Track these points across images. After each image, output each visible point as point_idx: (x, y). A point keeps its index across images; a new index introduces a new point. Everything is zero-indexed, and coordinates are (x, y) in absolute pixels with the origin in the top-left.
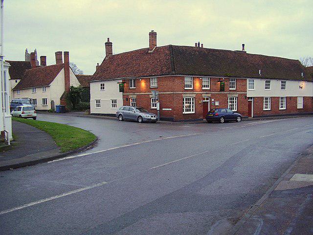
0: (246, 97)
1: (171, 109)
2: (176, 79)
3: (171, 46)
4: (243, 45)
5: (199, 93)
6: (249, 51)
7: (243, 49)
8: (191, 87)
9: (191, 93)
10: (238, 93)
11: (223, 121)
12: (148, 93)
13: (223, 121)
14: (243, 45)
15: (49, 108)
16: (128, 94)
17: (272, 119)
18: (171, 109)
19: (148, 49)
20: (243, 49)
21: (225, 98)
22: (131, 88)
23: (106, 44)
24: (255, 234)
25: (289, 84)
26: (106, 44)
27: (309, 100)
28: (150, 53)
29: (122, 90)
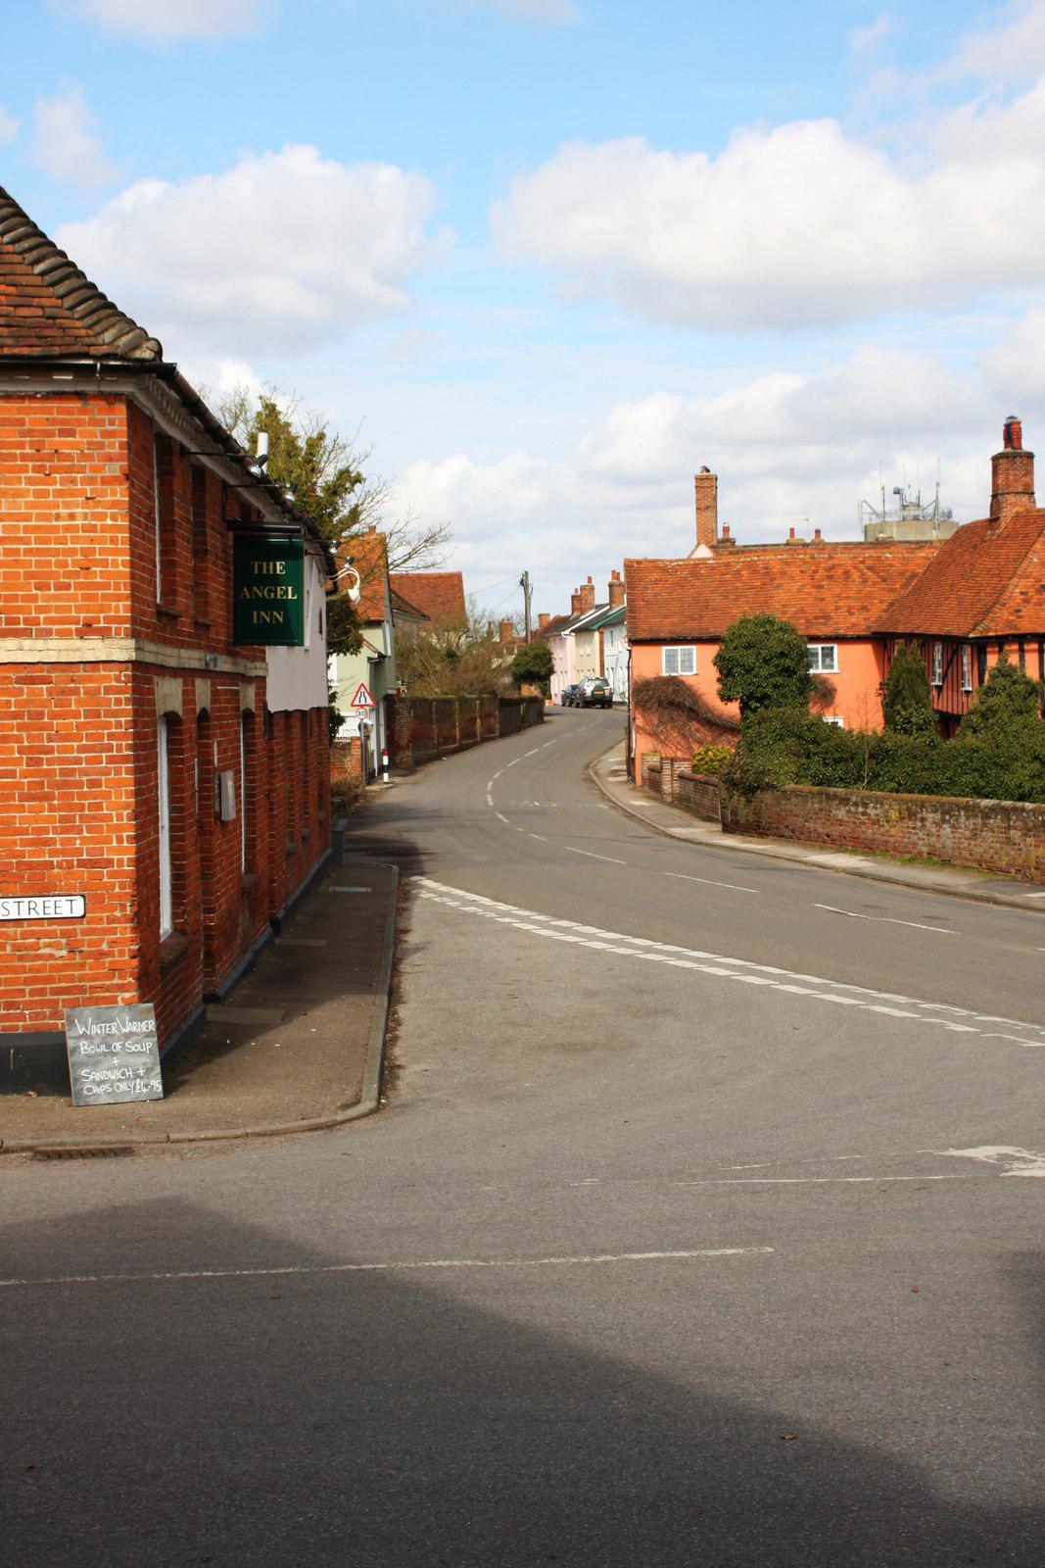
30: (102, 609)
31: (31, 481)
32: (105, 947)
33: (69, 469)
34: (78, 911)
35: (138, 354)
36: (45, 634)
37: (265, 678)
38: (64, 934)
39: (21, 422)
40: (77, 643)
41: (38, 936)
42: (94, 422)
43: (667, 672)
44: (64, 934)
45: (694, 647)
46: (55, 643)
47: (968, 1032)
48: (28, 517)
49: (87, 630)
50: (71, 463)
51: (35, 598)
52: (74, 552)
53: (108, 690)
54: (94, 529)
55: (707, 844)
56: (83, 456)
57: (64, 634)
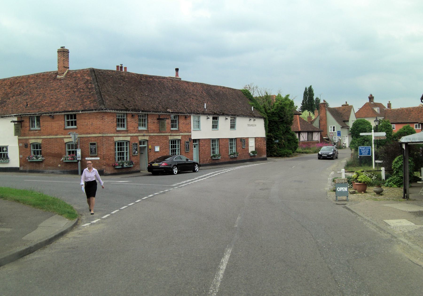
0: (190, 139)
1: (99, 158)
2: (106, 117)
3: (93, 71)
4: (177, 70)
5: (135, 135)
6: (184, 76)
7: (177, 75)
8: (176, 128)
9: (124, 135)
10: (181, 134)
11: (175, 171)
12: (62, 136)
13: (175, 171)
14: (177, 70)
15: (270, 155)
16: (28, 137)
17: (236, 166)
18: (99, 158)
19: (57, 74)
20: (177, 75)
21: (166, 141)
22: (32, 129)
23: (388, 104)
24: (421, 263)
25: (240, 122)
26: (388, 104)
27: (261, 141)
28: (60, 80)
29: (17, 132)
30: (101, 131)
31: (95, 120)
32: (101, 162)
33: (98, 119)
34: (99, 159)
35: (102, 108)
36: (96, 134)
37: (191, 135)
38: (98, 161)
39: (94, 115)
40: (99, 134)
41: (96, 161)
42: (100, 114)
43: (330, 131)
44: (98, 161)
45: (395, 125)
46: (97, 134)
47: (109, 216)
48: (95, 123)
49: (100, 133)
50: (15, 123)
51: (95, 130)
52: (98, 126)
53: (101, 139)
54: (100, 124)
55: (343, 154)
56: (99, 117)
57: (98, 134)
